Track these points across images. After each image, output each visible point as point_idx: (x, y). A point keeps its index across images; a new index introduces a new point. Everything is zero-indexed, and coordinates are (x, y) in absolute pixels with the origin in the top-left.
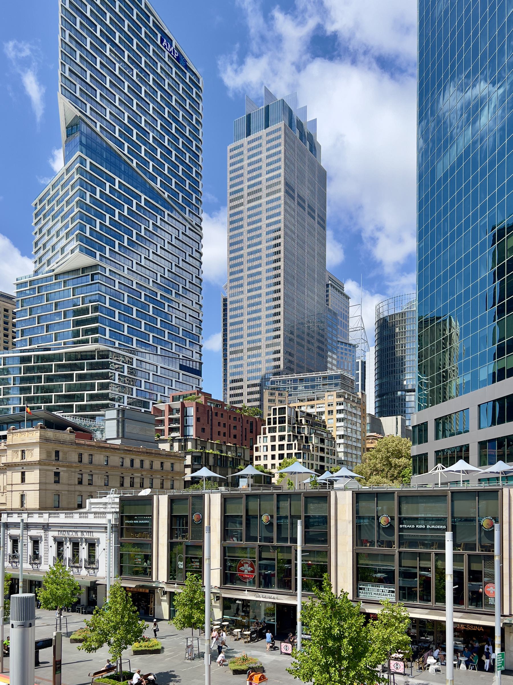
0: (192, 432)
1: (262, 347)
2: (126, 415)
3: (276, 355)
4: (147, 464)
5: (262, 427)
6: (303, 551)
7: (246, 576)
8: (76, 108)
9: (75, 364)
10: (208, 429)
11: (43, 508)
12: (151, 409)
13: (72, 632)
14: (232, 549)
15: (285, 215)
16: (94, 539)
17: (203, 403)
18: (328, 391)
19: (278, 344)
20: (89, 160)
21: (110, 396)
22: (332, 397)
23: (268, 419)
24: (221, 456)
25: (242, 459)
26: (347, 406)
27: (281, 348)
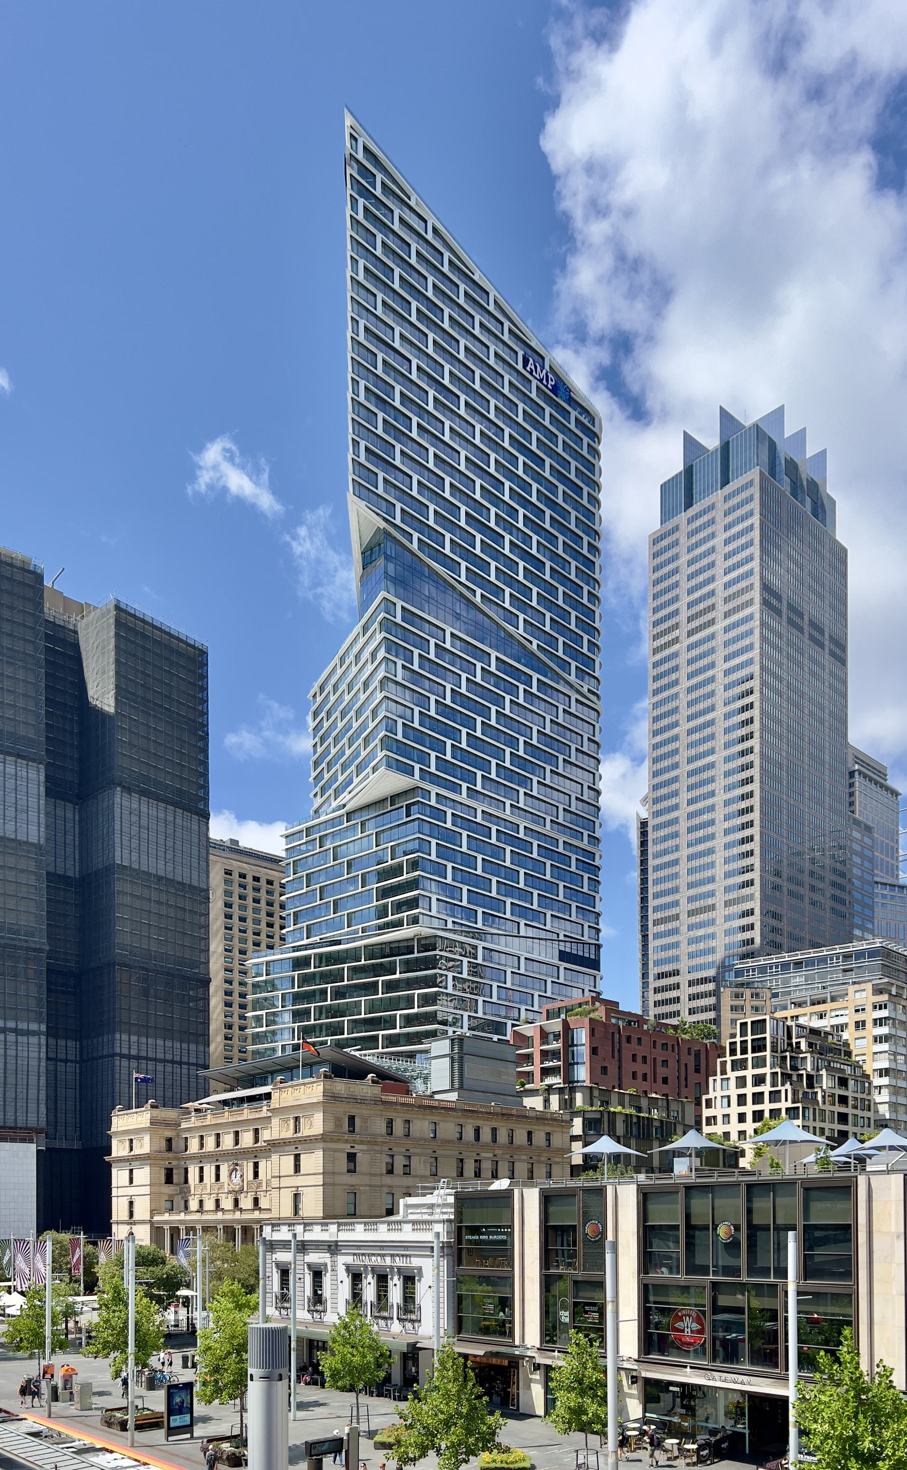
0: (582, 1073)
1: (717, 906)
2: (465, 1047)
3: (746, 918)
4: (503, 1137)
5: (719, 1060)
6: (799, 1293)
7: (688, 1339)
8: (378, 514)
9: (381, 964)
10: (613, 1069)
11: (329, 1215)
12: (509, 1037)
13: (377, 1430)
14: (663, 1288)
15: (761, 648)
16: (413, 1268)
17: (604, 1019)
18: (854, 983)
19: (751, 897)
20: (400, 604)
21: (440, 1017)
22: (864, 994)
23: (731, 1043)
24: (638, 1117)
25: (679, 1123)
26: (895, 1010)
27: (756, 905)
